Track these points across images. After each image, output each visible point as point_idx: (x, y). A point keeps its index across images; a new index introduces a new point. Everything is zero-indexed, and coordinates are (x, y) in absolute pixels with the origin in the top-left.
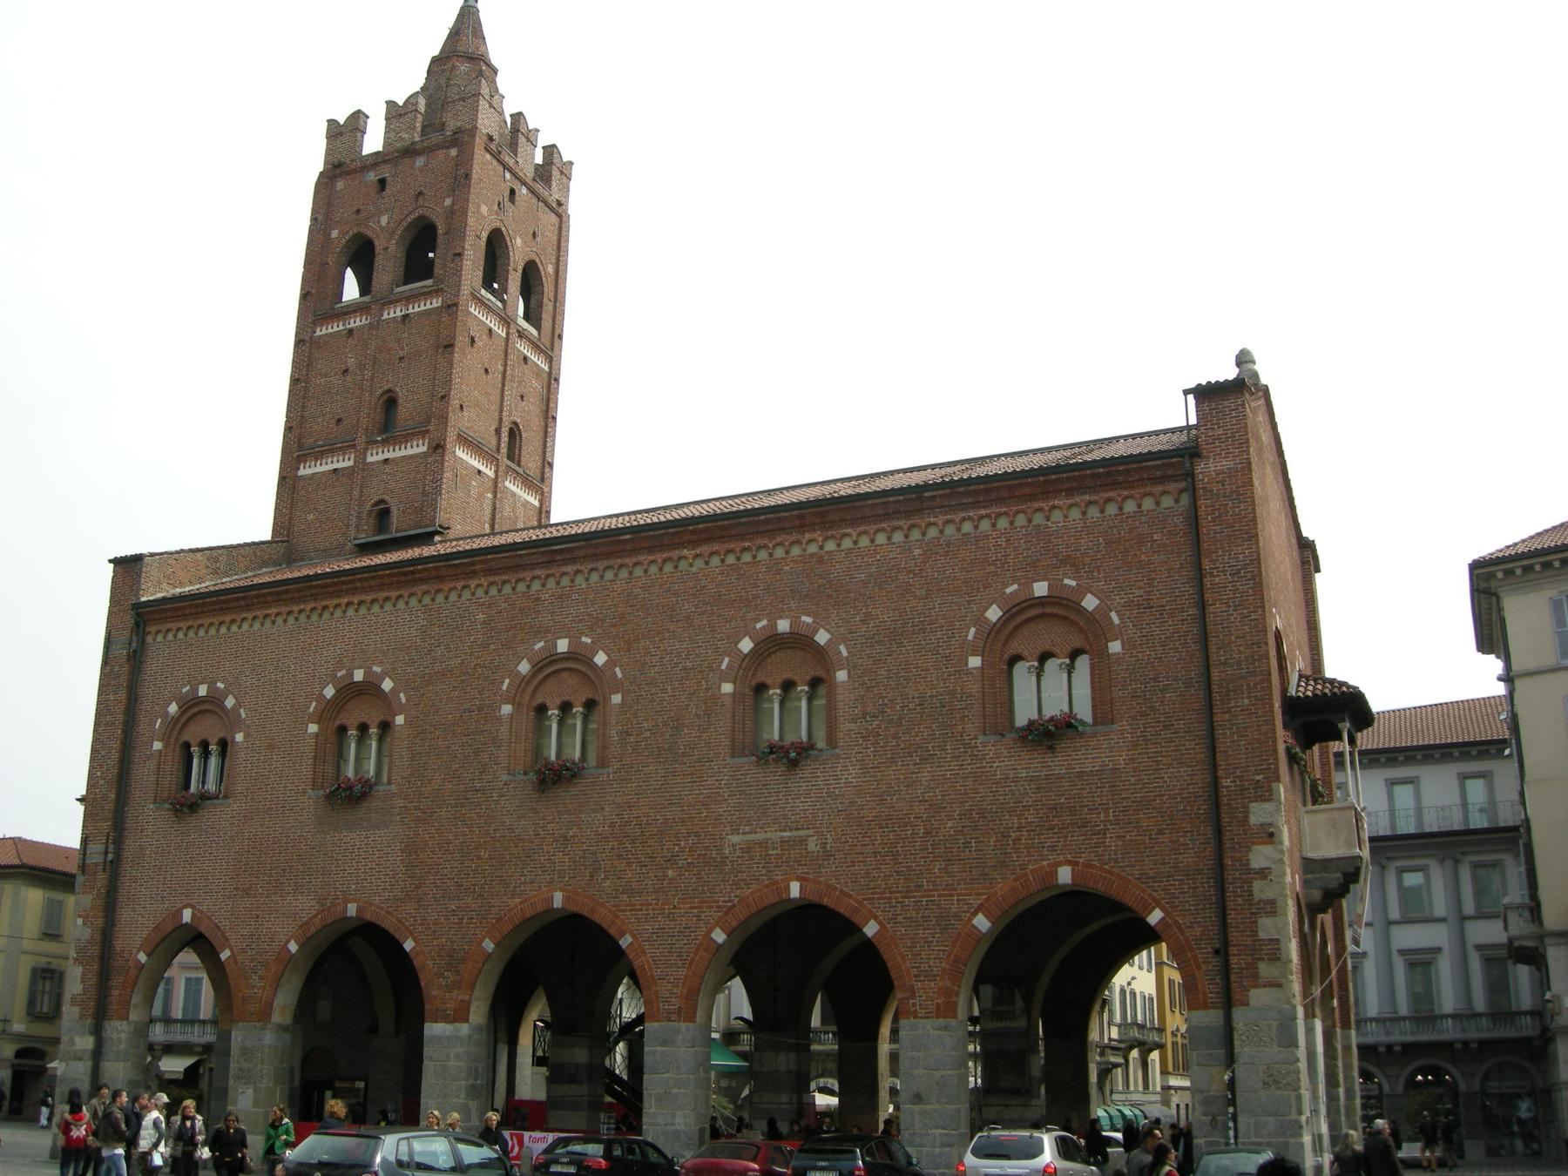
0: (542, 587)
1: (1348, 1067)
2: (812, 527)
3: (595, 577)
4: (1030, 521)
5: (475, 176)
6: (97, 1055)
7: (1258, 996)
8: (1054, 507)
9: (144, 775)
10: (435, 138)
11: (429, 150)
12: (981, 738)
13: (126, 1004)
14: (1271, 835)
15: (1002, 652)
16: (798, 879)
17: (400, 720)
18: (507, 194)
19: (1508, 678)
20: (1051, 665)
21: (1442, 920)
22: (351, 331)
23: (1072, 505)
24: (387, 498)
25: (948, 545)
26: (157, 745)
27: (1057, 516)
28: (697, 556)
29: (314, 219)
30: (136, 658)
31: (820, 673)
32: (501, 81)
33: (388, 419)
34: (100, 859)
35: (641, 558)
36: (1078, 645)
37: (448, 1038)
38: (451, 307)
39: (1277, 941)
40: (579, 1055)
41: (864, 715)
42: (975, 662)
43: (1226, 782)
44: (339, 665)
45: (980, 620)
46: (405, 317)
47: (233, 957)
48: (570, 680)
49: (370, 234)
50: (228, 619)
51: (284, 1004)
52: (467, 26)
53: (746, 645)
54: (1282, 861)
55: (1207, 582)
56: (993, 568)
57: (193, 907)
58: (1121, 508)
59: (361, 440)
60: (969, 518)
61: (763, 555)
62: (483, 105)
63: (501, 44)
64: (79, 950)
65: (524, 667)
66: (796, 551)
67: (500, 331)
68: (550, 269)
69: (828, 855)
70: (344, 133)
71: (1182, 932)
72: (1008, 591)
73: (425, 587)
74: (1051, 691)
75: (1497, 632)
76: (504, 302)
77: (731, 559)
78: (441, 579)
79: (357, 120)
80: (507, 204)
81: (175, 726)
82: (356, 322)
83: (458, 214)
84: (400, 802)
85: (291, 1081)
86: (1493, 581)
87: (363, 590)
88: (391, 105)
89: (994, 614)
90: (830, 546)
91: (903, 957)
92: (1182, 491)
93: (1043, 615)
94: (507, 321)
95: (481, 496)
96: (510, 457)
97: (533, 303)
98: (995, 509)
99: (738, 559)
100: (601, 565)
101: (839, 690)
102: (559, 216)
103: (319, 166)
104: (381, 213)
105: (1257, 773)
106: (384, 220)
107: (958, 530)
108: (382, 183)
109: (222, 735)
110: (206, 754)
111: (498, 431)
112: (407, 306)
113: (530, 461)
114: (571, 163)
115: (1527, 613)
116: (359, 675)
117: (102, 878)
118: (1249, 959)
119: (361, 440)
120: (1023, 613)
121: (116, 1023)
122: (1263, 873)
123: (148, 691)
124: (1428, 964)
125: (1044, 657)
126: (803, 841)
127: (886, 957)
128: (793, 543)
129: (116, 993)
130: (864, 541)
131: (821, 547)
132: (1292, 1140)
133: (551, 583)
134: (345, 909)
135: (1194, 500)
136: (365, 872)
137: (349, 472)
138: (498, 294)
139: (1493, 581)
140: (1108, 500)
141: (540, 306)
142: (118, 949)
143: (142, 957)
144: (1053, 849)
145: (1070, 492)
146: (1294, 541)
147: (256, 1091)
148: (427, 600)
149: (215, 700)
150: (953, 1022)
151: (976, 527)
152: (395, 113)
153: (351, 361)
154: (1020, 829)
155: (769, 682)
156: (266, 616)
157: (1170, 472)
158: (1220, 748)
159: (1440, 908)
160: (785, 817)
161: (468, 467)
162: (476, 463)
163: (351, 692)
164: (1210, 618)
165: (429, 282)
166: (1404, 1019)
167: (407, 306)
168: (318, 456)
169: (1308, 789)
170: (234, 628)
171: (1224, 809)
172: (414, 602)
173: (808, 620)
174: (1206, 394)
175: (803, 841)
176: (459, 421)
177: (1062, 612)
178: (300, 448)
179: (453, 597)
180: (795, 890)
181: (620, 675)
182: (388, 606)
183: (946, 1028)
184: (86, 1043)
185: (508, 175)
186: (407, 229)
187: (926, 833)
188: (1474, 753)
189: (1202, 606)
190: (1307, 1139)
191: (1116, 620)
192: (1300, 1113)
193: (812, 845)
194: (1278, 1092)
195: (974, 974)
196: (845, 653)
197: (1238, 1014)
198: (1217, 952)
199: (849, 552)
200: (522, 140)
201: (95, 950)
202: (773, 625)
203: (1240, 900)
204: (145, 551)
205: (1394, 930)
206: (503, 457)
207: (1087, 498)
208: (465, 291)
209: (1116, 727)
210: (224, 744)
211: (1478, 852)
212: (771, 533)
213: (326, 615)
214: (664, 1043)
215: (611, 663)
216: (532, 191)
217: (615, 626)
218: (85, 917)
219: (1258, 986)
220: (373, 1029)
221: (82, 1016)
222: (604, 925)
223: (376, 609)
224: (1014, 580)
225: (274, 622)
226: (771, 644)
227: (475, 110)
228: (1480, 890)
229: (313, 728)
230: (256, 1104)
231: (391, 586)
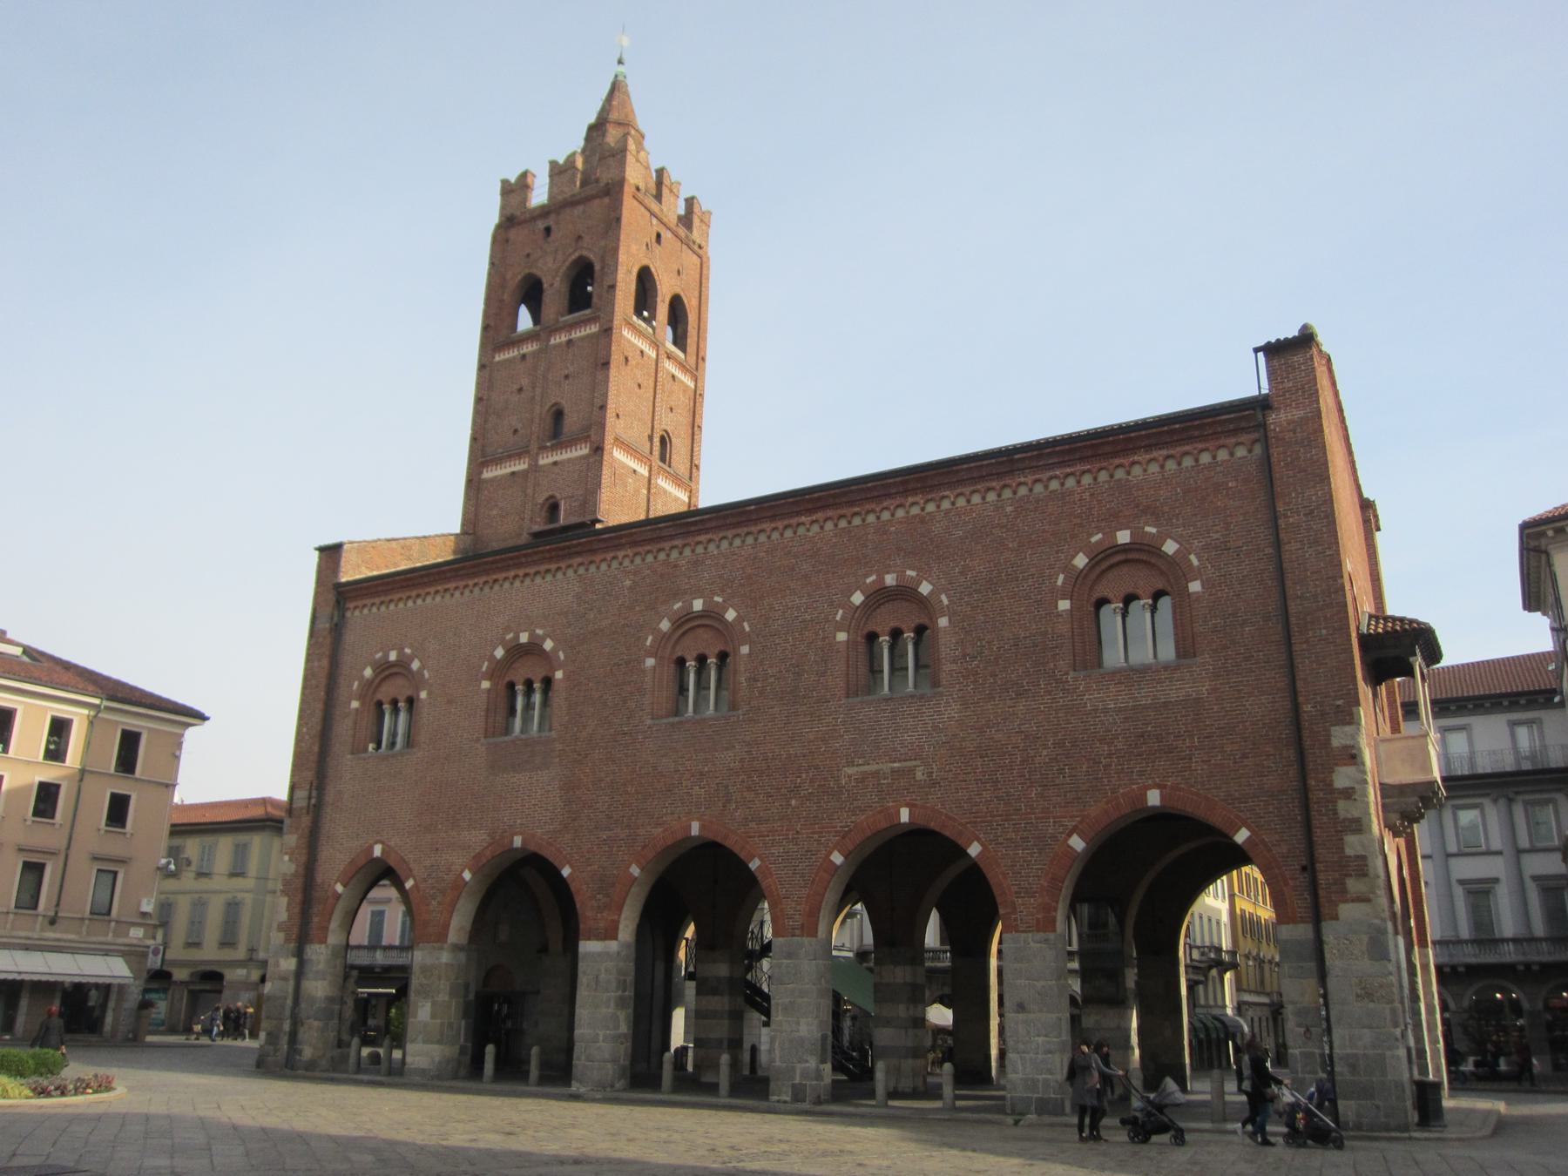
0: (680, 555)
1: (1427, 984)
2: (914, 491)
3: (725, 544)
4: (1112, 476)
7: (1346, 910)
8: (1134, 463)
9: (343, 729)
10: (590, 190)
11: (587, 199)
12: (1072, 674)
13: (325, 929)
14: (1354, 757)
15: (1091, 588)
16: (907, 805)
17: (559, 675)
20: (1135, 606)
21: (1499, 853)
22: (524, 357)
23: (1151, 460)
25: (1037, 501)
26: (355, 704)
28: (813, 522)
29: (492, 264)
30: (337, 630)
31: (924, 621)
32: (647, 144)
33: (556, 428)
34: (304, 803)
35: (764, 526)
36: (1160, 586)
37: (599, 954)
38: (607, 331)
39: (1364, 858)
40: (722, 970)
41: (964, 656)
43: (1308, 708)
44: (508, 629)
45: (1067, 568)
46: (570, 342)
47: (416, 886)
48: (704, 634)
49: (538, 273)
50: (414, 594)
51: (459, 924)
52: (616, 87)
53: (858, 598)
54: (1365, 782)
55: (1281, 522)
58: (1197, 460)
59: (534, 447)
60: (1056, 477)
61: (871, 518)
62: (630, 159)
63: (645, 110)
64: (286, 883)
65: (665, 625)
66: (900, 513)
68: (694, 302)
69: (934, 784)
70: (514, 190)
71: (1270, 851)
73: (579, 560)
74: (1138, 639)
76: (654, 328)
77: (843, 524)
78: (593, 551)
81: (370, 687)
82: (528, 348)
84: (559, 746)
85: (466, 996)
86: (1542, 540)
87: (528, 564)
88: (553, 164)
89: (1081, 561)
90: (931, 507)
92: (1255, 441)
93: (1126, 561)
94: (656, 345)
95: (637, 491)
96: (663, 459)
97: (680, 331)
98: (1079, 467)
100: (730, 534)
101: (941, 635)
102: (700, 257)
103: (495, 218)
107: (1046, 487)
108: (548, 230)
109: (409, 693)
110: (396, 711)
111: (651, 438)
114: (710, 213)
116: (524, 638)
117: (306, 821)
118: (1337, 875)
119: (534, 447)
120: (1108, 559)
121: (316, 947)
122: (1348, 793)
123: (347, 659)
124: (1487, 893)
125: (1128, 599)
126: (912, 771)
127: (989, 876)
129: (316, 919)
130: (961, 502)
131: (923, 509)
132: (1388, 1053)
133: (687, 551)
135: (1267, 448)
136: (530, 812)
137: (524, 474)
138: (648, 321)
139: (1542, 540)
142: (319, 880)
143: (339, 888)
144: (1141, 773)
145: (1149, 448)
146: (1356, 500)
147: (434, 1004)
148: (581, 571)
150: (1052, 936)
151: (1062, 484)
152: (558, 171)
154: (1110, 755)
155: (879, 630)
157: (1243, 424)
158: (1300, 675)
160: (894, 750)
161: (624, 466)
162: (632, 464)
163: (517, 652)
164: (1286, 556)
165: (588, 311)
166: (1466, 942)
168: (498, 461)
171: (1305, 733)
172: (570, 572)
174: (1273, 350)
175: (912, 771)
176: (614, 427)
177: (1144, 557)
178: (483, 456)
179: (604, 567)
180: (905, 816)
181: (747, 629)
182: (549, 577)
183: (1046, 941)
185: (655, 221)
186: (569, 268)
187: (1022, 762)
188: (1523, 702)
189: (1278, 544)
190: (1402, 1052)
191: (1195, 562)
193: (919, 775)
194: (1371, 1005)
195: (1071, 891)
196: (946, 601)
197: (1328, 929)
198: (1304, 869)
199: (947, 512)
200: (665, 191)
201: (299, 883)
202: (881, 579)
203: (1325, 819)
204: (344, 540)
205: (1453, 861)
206: (657, 462)
207: (1165, 452)
209: (1198, 660)
210: (411, 701)
211: (1532, 792)
212: (879, 498)
213: (497, 587)
214: (789, 956)
215: (740, 619)
217: (742, 585)
218: (291, 854)
219: (1346, 901)
220: (544, 950)
221: (287, 940)
222: (736, 850)
223: (538, 580)
224: (1099, 529)
226: (880, 596)
227: (622, 164)
228: (1533, 825)
229: (486, 685)
230: (433, 1016)
231: (550, 560)
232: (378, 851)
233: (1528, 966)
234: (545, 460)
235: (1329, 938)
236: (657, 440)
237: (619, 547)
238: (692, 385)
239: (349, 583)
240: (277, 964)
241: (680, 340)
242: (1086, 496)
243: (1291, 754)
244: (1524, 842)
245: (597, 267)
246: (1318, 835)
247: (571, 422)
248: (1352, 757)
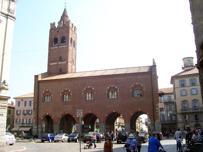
6: (38, 128)
7: (157, 120)
9: (40, 99)
16: (115, 110)
22: (55, 49)
26: (42, 96)
27: (139, 77)
30: (38, 86)
33: (61, 59)
42: (131, 90)
44: (64, 88)
49: (57, 37)
52: (65, 10)
65: (85, 89)
70: (53, 25)
79: (54, 23)
83: (68, 36)
89: (133, 86)
103: (50, 28)
104: (58, 35)
106: (59, 36)
108: (58, 31)
113: (74, 63)
115: (177, 82)
116: (66, 89)
120: (135, 86)
122: (157, 110)
126: (114, 107)
135: (152, 76)
143: (42, 118)
149: (49, 91)
153: (56, 52)
165: (64, 44)
169: (73, 42)
180: (114, 111)
184: (36, 127)
206: (72, 63)
208: (69, 45)
216: (74, 32)
218: (35, 114)
220: (64, 125)
221: (35, 125)
232: (47, 114)
233: (168, 124)
234: (59, 63)
237: (79, 79)
239: (39, 81)
241: (74, 46)
243: (152, 106)
244: (168, 110)
245: (66, 38)
246: (155, 114)
247: (63, 58)
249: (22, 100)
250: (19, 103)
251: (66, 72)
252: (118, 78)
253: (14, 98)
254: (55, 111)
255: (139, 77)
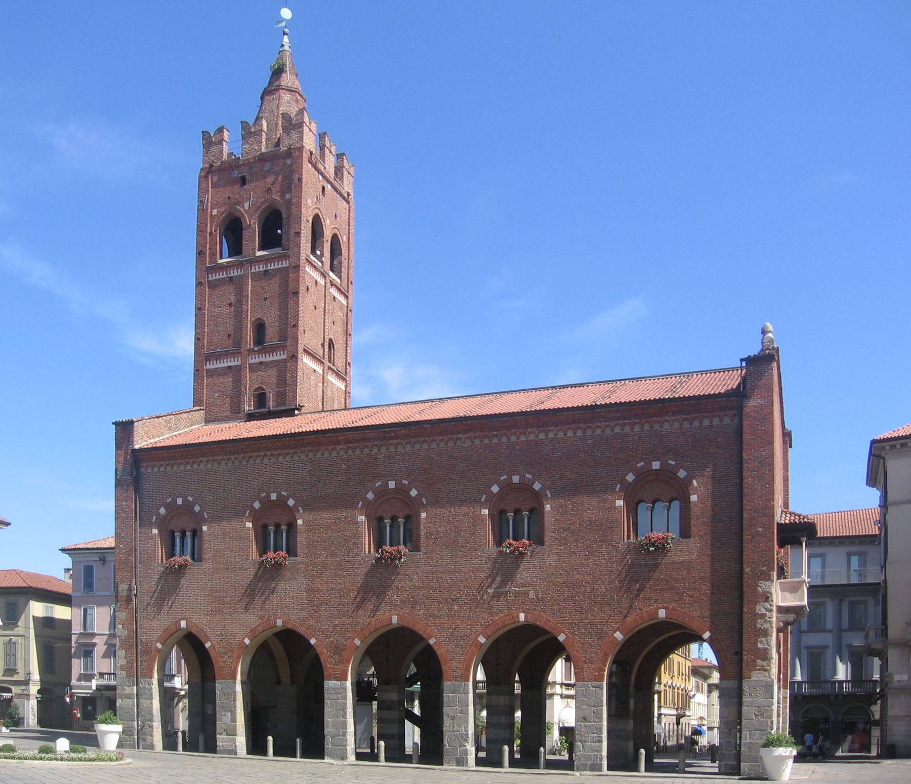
4: (652, 427)
5: (304, 180)
8: (665, 421)
14: (768, 598)
18: (321, 190)
19: (885, 504)
21: (830, 631)
22: (231, 278)
23: (675, 420)
24: (265, 387)
27: (666, 426)
43: (747, 570)
44: (261, 490)
46: (266, 271)
56: (631, 453)
57: (186, 619)
61: (504, 439)
66: (523, 438)
67: (321, 281)
68: (345, 239)
72: (638, 465)
73: (310, 448)
75: (881, 476)
77: (486, 441)
80: (322, 197)
86: (881, 454)
90: (542, 436)
91: (578, 651)
92: (734, 415)
94: (324, 275)
95: (316, 385)
99: (490, 441)
105: (763, 566)
106: (246, 205)
109: (194, 526)
111: (323, 345)
112: (266, 264)
113: (340, 364)
120: (645, 477)
122: (763, 616)
126: (526, 594)
128: (521, 433)
131: (537, 437)
134: (276, 622)
140: (695, 418)
141: (340, 263)
143: (159, 646)
144: (656, 601)
151: (622, 429)
155: (507, 509)
156: (214, 460)
159: (830, 623)
164: (745, 485)
167: (266, 264)
170: (195, 466)
173: (530, 476)
186: (262, 212)
189: (741, 478)
192: (772, 729)
193: (532, 595)
198: (736, 653)
199: (553, 439)
210: (196, 533)
215: (419, 496)
220: (278, 682)
223: (281, 459)
225: (219, 464)
235: (745, 687)
236: (327, 344)
237: (338, 442)
238: (345, 303)
239: (141, 450)
240: (123, 689)
242: (636, 438)
244: (845, 624)
247: (271, 333)
248: (767, 598)
249: (103, 560)
250: (89, 571)
251: (285, 405)
252: (551, 435)
253: (63, 550)
254: (218, 611)
255: (671, 426)
